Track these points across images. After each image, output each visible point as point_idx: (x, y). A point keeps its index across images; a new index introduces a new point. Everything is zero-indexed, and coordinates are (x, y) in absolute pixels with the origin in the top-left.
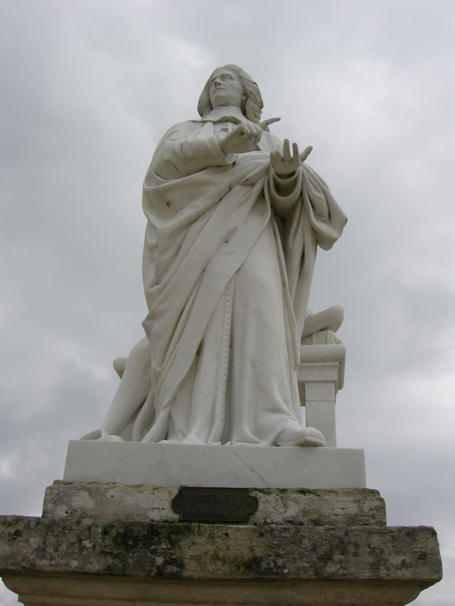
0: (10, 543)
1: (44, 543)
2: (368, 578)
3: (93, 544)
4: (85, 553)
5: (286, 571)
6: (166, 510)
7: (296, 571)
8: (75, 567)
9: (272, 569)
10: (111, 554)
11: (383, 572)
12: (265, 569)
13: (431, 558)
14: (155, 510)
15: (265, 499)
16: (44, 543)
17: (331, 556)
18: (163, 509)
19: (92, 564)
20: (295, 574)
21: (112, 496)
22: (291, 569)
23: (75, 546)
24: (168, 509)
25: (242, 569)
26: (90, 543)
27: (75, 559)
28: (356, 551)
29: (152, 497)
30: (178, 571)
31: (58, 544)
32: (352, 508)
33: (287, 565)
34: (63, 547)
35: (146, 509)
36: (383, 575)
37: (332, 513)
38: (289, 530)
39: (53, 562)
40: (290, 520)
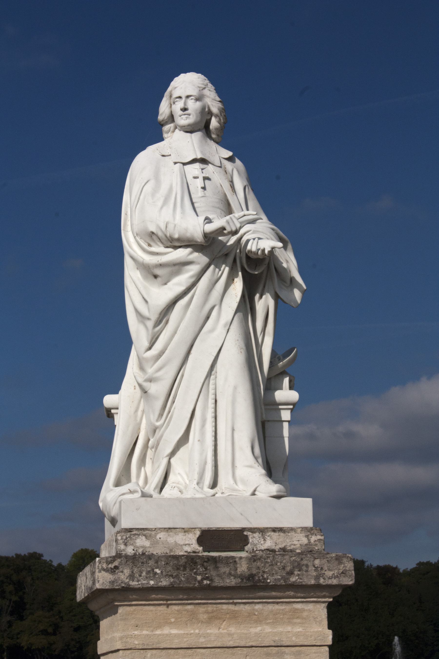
0: (112, 574)
1: (132, 572)
2: (313, 584)
3: (161, 571)
4: (157, 576)
5: (269, 581)
6: (194, 545)
7: (274, 581)
8: (152, 584)
9: (261, 580)
10: (172, 576)
11: (322, 581)
12: (257, 580)
13: (349, 573)
14: (187, 545)
15: (252, 536)
16: (132, 572)
17: (293, 572)
18: (192, 544)
19: (162, 582)
20: (273, 582)
21: (160, 538)
22: (271, 579)
23: (151, 573)
24: (195, 544)
25: (245, 581)
26: (159, 570)
27: (152, 580)
28: (307, 569)
29: (184, 537)
30: (210, 583)
31: (141, 572)
32: (304, 540)
33: (269, 577)
34: (144, 574)
35: (182, 545)
36: (321, 582)
37: (292, 544)
38: (270, 558)
39: (140, 583)
40: (267, 548)
